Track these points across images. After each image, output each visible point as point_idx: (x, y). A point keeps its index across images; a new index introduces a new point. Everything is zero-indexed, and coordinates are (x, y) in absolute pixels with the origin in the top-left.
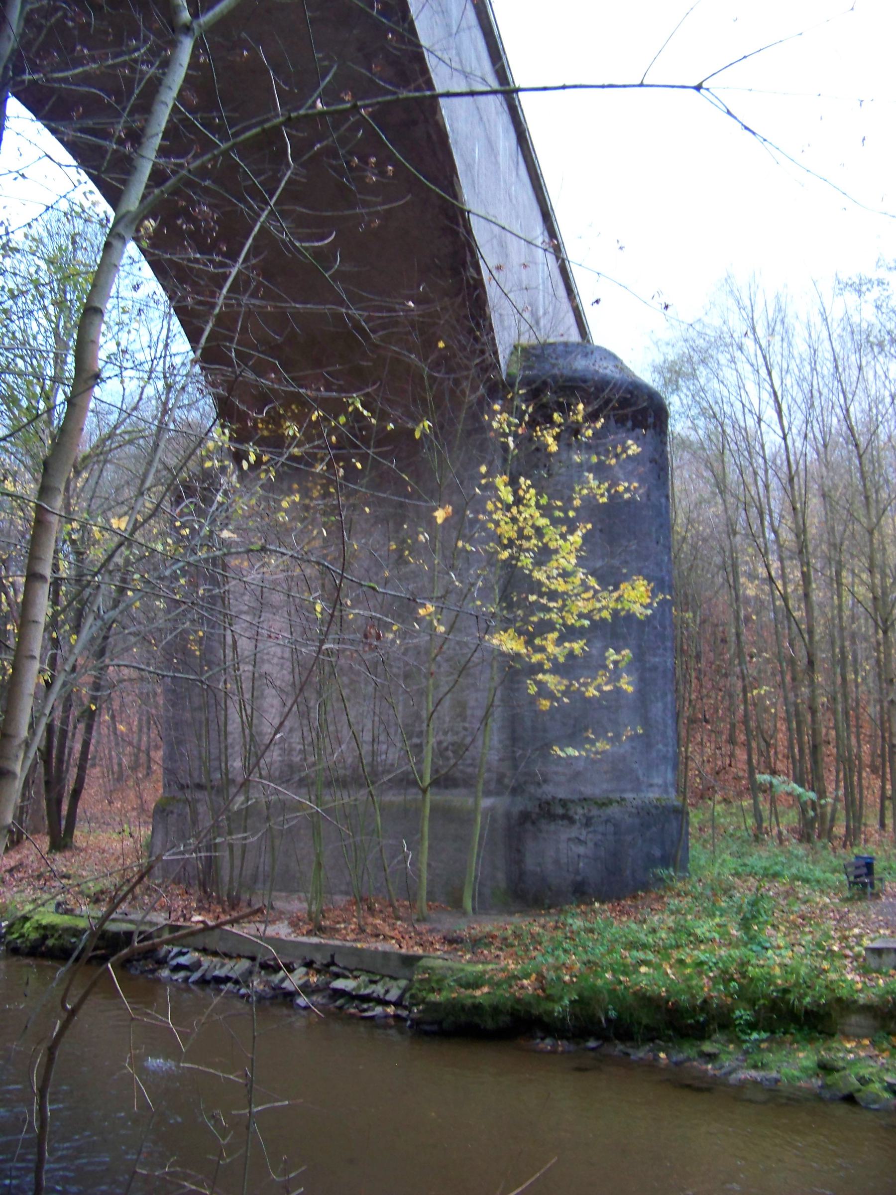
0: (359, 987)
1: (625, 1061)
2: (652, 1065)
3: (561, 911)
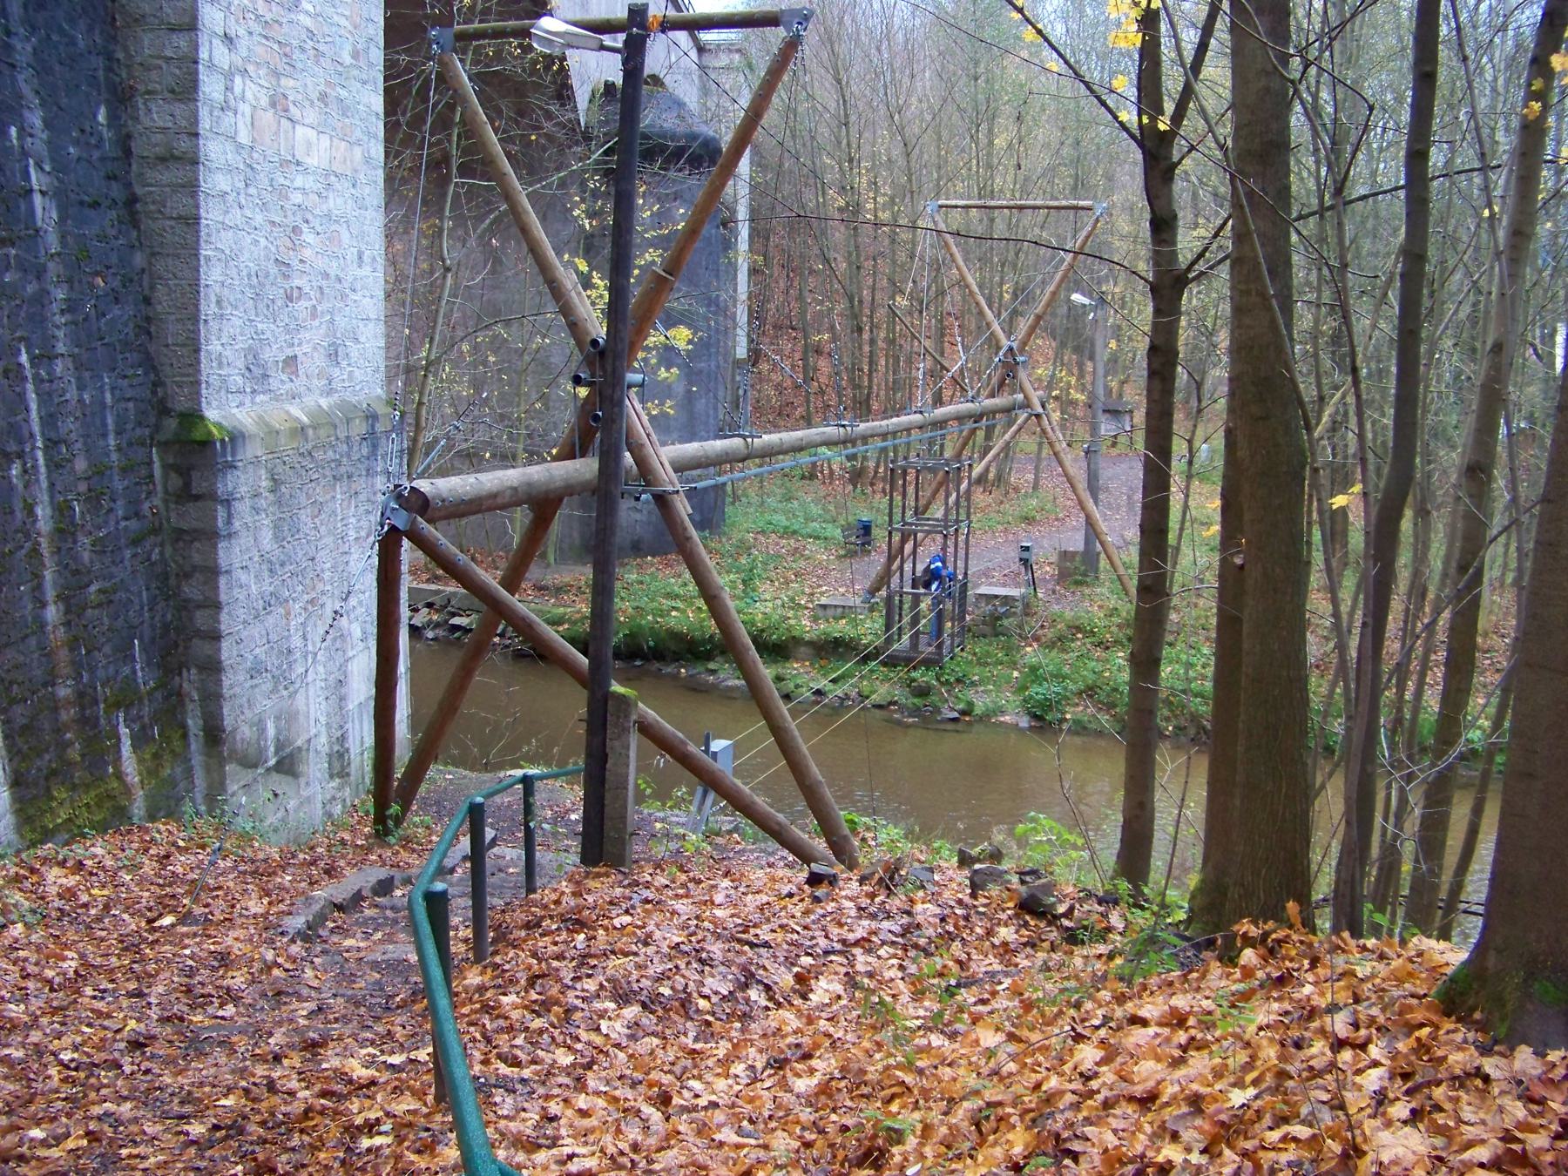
1: (658, 675)
2: (676, 677)
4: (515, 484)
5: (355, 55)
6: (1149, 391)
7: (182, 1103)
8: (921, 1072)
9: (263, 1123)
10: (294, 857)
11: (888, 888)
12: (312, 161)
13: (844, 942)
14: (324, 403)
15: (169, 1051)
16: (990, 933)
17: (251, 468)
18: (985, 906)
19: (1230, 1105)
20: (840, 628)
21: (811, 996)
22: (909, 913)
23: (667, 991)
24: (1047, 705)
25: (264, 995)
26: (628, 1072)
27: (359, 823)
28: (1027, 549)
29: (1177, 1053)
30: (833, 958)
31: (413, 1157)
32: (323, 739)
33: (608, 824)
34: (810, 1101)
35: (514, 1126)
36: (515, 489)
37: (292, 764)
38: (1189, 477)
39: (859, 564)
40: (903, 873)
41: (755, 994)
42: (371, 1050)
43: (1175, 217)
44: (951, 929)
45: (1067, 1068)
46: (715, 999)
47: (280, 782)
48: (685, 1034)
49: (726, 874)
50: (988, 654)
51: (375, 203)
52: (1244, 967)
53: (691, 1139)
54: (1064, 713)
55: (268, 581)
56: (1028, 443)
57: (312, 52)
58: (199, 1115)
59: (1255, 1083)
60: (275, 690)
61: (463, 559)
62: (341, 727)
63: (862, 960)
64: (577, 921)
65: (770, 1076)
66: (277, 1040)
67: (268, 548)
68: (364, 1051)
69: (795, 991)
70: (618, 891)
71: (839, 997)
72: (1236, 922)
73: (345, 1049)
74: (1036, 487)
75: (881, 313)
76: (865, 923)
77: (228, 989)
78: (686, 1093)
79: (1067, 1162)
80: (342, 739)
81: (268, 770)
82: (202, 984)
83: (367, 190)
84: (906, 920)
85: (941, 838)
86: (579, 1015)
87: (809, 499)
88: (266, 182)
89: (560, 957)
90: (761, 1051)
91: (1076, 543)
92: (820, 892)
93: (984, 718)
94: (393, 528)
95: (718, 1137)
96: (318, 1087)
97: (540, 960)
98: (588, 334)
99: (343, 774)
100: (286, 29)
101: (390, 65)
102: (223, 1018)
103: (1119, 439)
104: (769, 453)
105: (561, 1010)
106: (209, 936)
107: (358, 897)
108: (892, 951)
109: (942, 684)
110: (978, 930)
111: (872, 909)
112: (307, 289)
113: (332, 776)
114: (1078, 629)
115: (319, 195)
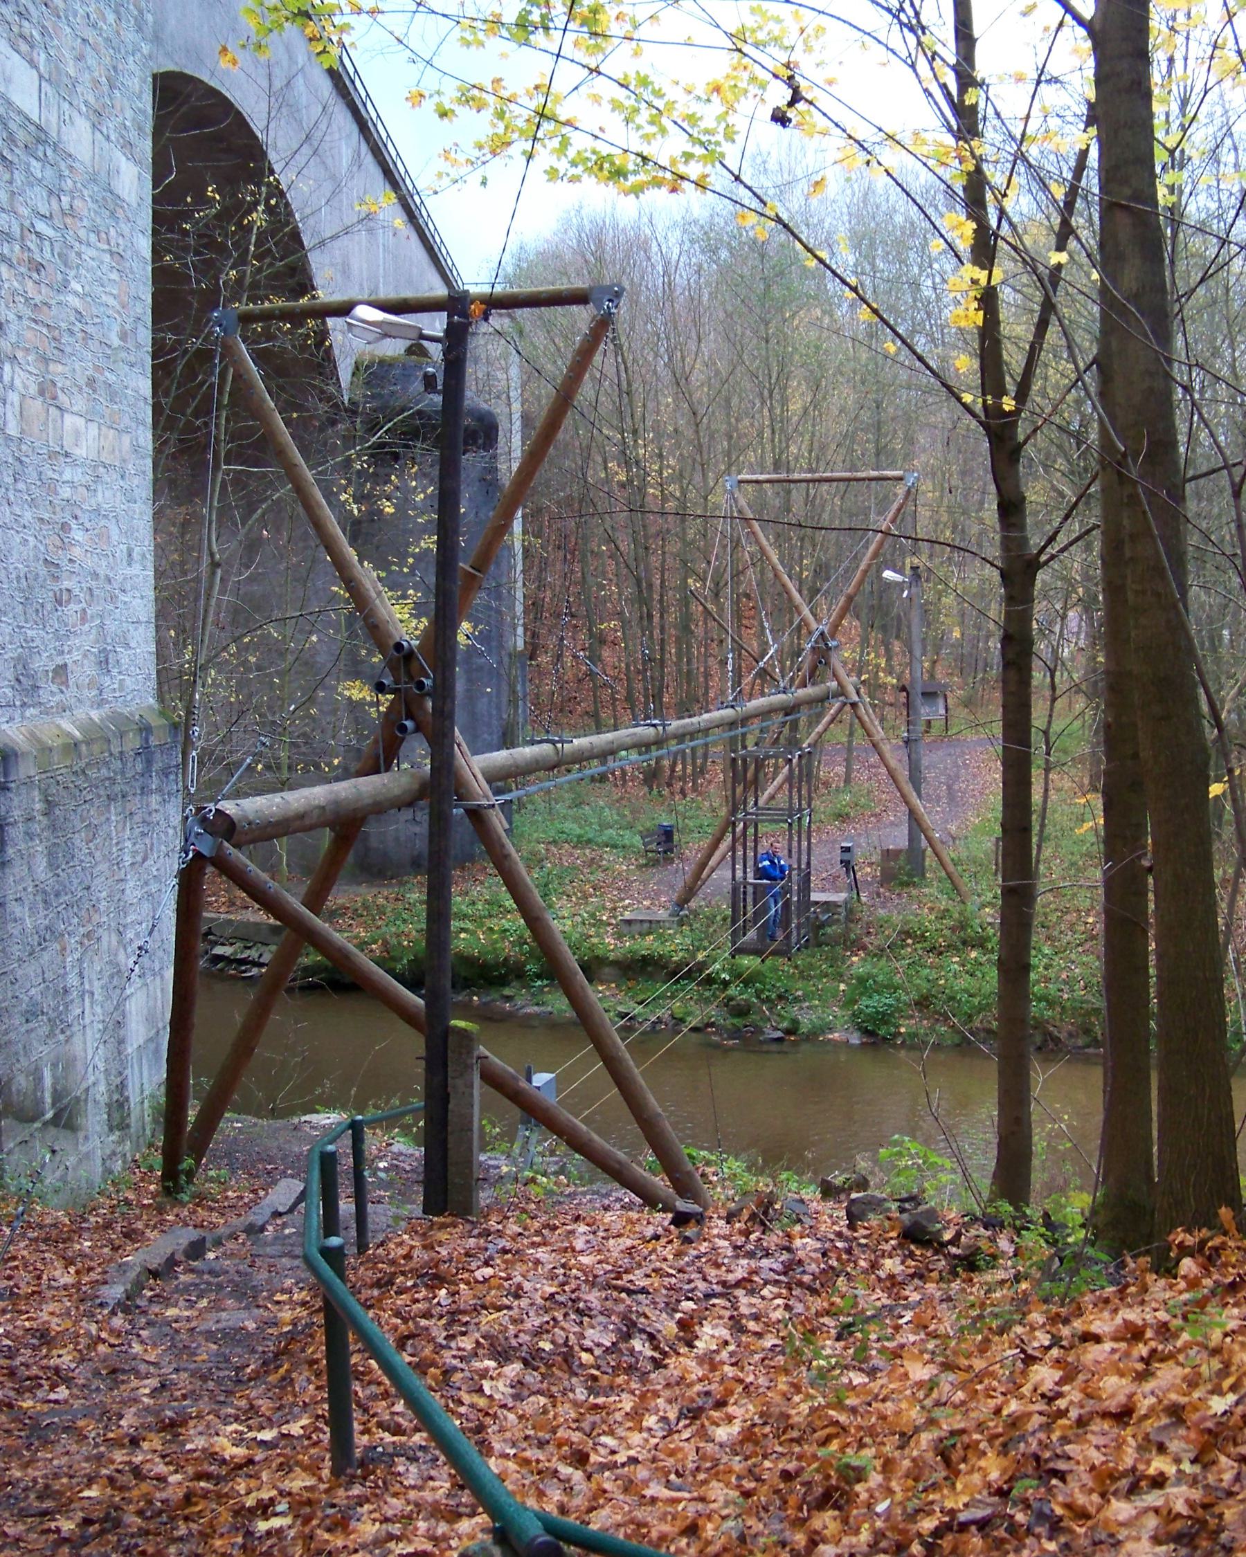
0: (235, 953)
3: (401, 884)
4: (322, 802)
5: (123, 336)
6: (1004, 681)
7: (40, 1498)
8: (854, 1410)
9: (140, 1513)
10: (86, 1220)
11: (763, 1224)
12: (80, 452)
13: (724, 1284)
14: (95, 715)
15: (8, 1442)
16: (874, 1266)
17: (23, 790)
18: (865, 1237)
19: (1211, 1412)
20: (648, 945)
21: (697, 1343)
22: (788, 1249)
23: (547, 1346)
24: (883, 1018)
25: (97, 1373)
26: (532, 1432)
27: (142, 1180)
28: (847, 850)
29: (1140, 1366)
30: (715, 1301)
31: (326, 1536)
32: (102, 1088)
33: (452, 1169)
34: (734, 1448)
35: (427, 1495)
36: (323, 808)
37: (70, 1117)
38: (1047, 770)
39: (656, 876)
40: (777, 1207)
41: (637, 1344)
42: (235, 1426)
43: (1024, 498)
44: (835, 1264)
45: (1026, 1390)
46: (597, 1352)
47: (62, 1140)
48: (573, 1391)
49: (577, 1219)
50: (811, 966)
51: (144, 495)
52: (1184, 1277)
53: (621, 1497)
54: (898, 1027)
55: (42, 913)
56: (839, 734)
57: (80, 335)
58: (64, 1508)
59: (1233, 1388)
60: (51, 1035)
61: (273, 885)
62: (120, 1074)
63: (746, 1303)
64: (436, 1276)
65: (686, 1427)
66: (128, 1422)
67: (42, 877)
68: (230, 1428)
69: (680, 1339)
70: (472, 1242)
71: (726, 1343)
72: (1170, 1233)
73: (208, 1426)
74: (847, 780)
75: (673, 596)
76: (744, 1262)
77: (57, 1370)
78: (602, 1451)
79: (1054, 1482)
80: (122, 1087)
81: (45, 1124)
82: (27, 1366)
83: (136, 481)
84: (785, 1256)
85: (788, 1169)
86: (459, 1375)
87: (602, 804)
88: (35, 475)
89: (427, 1315)
90: (670, 1402)
91: (899, 839)
92: (690, 1232)
93: (811, 1036)
94: (198, 855)
95: (648, 1492)
96: (190, 1470)
97: (405, 1321)
98: (390, 636)
99: (123, 1126)
100: (54, 311)
101: (158, 350)
102: (56, 1402)
103: (923, 728)
104: (581, 758)
105: (438, 1372)
106: (21, 1312)
107: (171, 1262)
108: (775, 1290)
109: (763, 1001)
110: (862, 1263)
111: (750, 1247)
112: (76, 591)
113: (111, 1129)
114: (908, 934)
115: (88, 488)
